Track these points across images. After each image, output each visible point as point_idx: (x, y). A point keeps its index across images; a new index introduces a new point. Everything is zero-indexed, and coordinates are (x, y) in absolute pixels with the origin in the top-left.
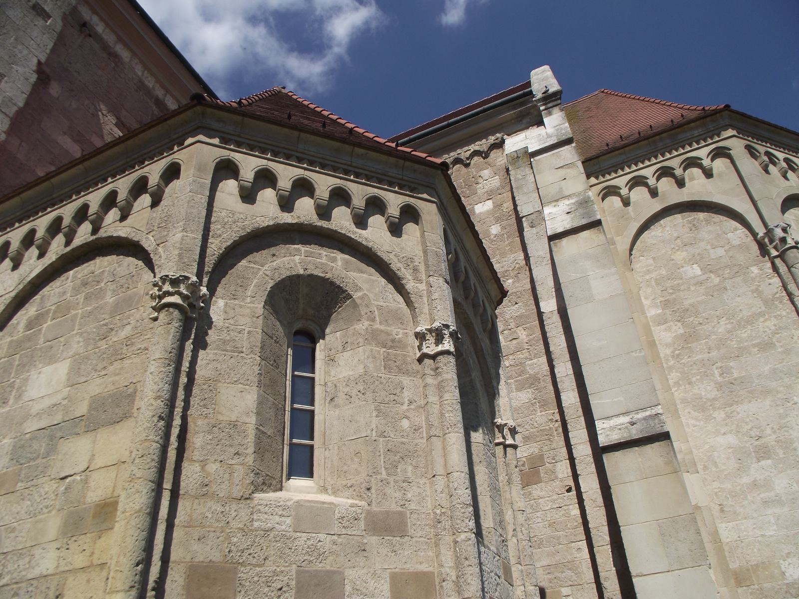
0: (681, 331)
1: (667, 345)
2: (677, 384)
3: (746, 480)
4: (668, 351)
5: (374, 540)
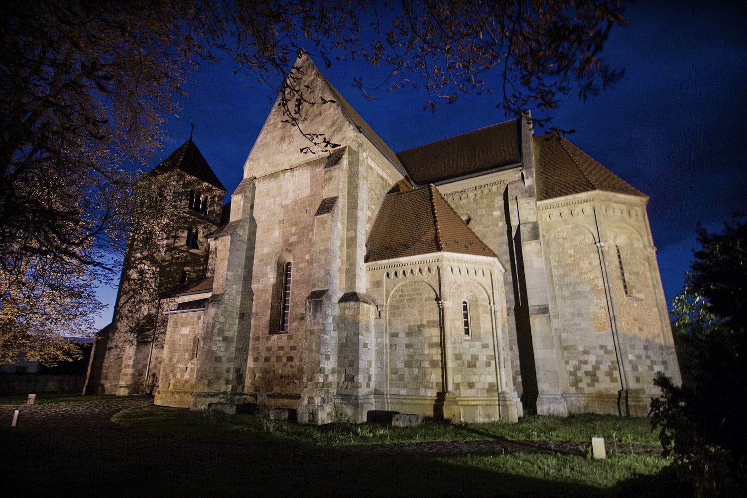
0: (562, 272)
1: (557, 276)
2: (558, 290)
3: (573, 322)
4: (557, 278)
5: (483, 349)
